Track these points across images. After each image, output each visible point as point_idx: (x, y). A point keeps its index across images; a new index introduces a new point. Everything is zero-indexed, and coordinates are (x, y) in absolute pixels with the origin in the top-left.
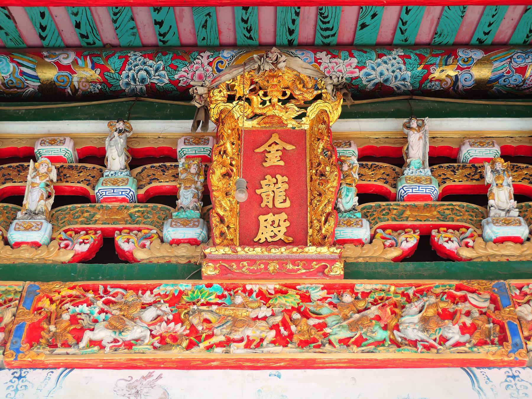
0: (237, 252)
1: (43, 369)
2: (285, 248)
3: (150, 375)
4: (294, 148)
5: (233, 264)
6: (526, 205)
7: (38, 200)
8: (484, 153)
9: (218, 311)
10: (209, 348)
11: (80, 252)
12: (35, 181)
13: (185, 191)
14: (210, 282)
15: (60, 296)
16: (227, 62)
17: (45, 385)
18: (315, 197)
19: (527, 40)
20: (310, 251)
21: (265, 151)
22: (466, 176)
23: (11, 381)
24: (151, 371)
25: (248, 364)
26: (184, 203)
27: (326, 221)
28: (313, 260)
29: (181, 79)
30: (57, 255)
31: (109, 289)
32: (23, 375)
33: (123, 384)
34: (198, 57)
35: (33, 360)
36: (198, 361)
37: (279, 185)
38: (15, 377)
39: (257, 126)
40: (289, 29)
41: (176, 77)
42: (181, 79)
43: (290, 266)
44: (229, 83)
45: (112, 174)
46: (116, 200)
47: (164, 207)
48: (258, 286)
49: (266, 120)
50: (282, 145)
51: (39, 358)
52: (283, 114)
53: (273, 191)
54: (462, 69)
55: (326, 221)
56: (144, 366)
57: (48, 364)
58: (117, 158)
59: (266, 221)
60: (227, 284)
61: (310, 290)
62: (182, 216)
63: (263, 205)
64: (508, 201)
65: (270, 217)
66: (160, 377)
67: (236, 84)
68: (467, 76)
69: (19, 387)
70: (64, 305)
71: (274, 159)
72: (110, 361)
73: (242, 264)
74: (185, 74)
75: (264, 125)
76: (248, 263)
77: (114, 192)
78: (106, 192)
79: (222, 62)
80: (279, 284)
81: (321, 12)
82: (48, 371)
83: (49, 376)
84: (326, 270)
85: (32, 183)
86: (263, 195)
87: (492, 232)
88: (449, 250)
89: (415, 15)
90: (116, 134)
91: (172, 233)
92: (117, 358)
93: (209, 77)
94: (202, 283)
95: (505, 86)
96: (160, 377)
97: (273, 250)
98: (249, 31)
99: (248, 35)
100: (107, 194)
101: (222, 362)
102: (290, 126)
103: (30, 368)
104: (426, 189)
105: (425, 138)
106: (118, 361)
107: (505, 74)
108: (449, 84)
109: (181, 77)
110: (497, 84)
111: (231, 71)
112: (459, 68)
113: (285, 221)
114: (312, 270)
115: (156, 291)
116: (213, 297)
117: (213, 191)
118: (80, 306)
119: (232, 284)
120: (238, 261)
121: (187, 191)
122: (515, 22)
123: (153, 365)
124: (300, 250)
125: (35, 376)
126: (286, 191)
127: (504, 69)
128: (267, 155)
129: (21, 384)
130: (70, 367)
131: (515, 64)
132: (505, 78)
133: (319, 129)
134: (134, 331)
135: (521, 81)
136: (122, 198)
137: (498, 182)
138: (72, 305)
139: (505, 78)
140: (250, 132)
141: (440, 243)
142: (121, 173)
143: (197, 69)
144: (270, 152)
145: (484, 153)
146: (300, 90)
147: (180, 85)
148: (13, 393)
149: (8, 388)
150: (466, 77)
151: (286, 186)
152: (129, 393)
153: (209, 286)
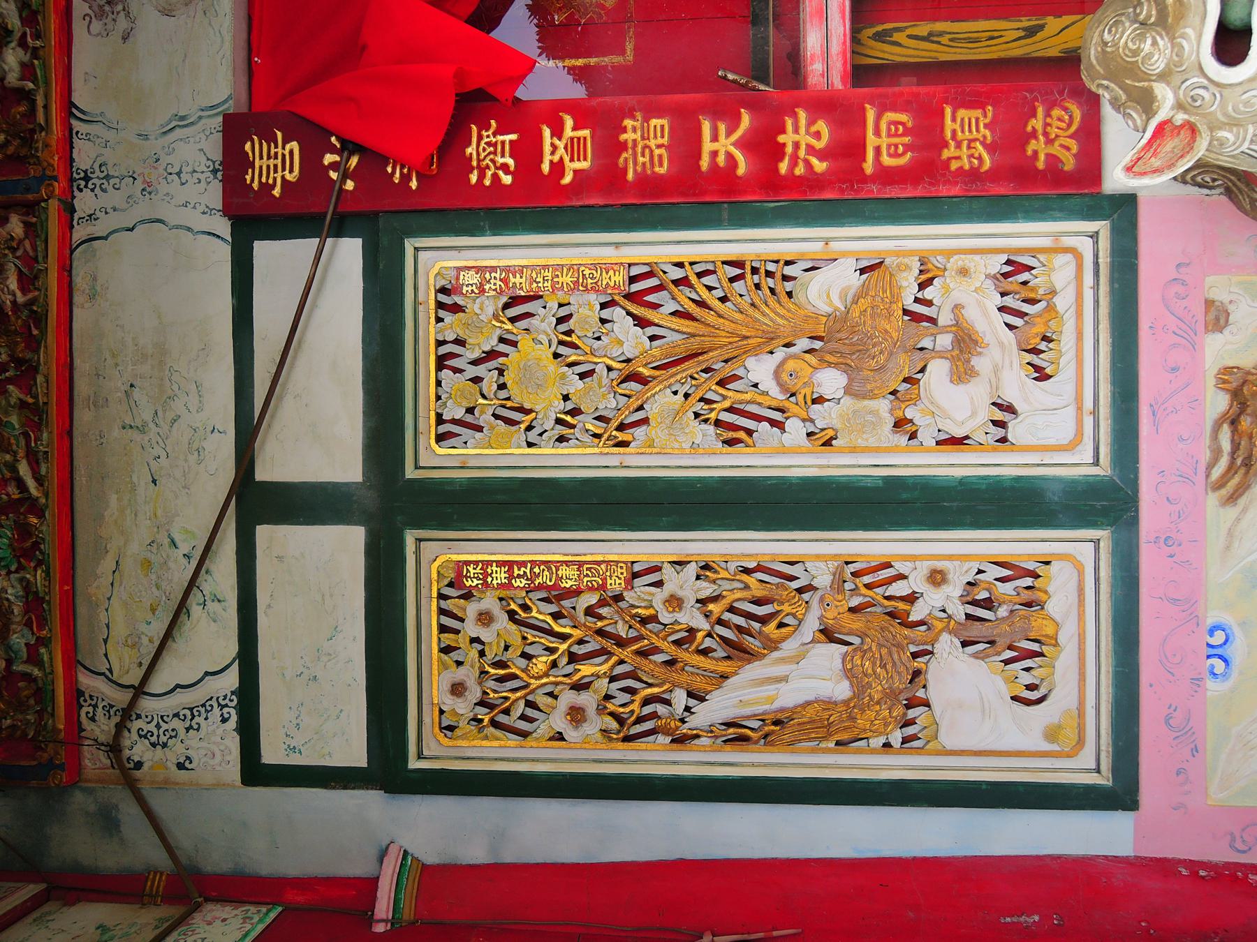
1: (72, 147)
6: (852, 573)
23: (92, 190)
32: (82, 175)
33: (96, 26)
38: (86, 186)
69: (102, 175)
82: (75, 140)
103: (72, 167)
105: (749, 616)
125: (84, 155)
129: (98, 173)
148: (112, 181)
149: (104, 191)
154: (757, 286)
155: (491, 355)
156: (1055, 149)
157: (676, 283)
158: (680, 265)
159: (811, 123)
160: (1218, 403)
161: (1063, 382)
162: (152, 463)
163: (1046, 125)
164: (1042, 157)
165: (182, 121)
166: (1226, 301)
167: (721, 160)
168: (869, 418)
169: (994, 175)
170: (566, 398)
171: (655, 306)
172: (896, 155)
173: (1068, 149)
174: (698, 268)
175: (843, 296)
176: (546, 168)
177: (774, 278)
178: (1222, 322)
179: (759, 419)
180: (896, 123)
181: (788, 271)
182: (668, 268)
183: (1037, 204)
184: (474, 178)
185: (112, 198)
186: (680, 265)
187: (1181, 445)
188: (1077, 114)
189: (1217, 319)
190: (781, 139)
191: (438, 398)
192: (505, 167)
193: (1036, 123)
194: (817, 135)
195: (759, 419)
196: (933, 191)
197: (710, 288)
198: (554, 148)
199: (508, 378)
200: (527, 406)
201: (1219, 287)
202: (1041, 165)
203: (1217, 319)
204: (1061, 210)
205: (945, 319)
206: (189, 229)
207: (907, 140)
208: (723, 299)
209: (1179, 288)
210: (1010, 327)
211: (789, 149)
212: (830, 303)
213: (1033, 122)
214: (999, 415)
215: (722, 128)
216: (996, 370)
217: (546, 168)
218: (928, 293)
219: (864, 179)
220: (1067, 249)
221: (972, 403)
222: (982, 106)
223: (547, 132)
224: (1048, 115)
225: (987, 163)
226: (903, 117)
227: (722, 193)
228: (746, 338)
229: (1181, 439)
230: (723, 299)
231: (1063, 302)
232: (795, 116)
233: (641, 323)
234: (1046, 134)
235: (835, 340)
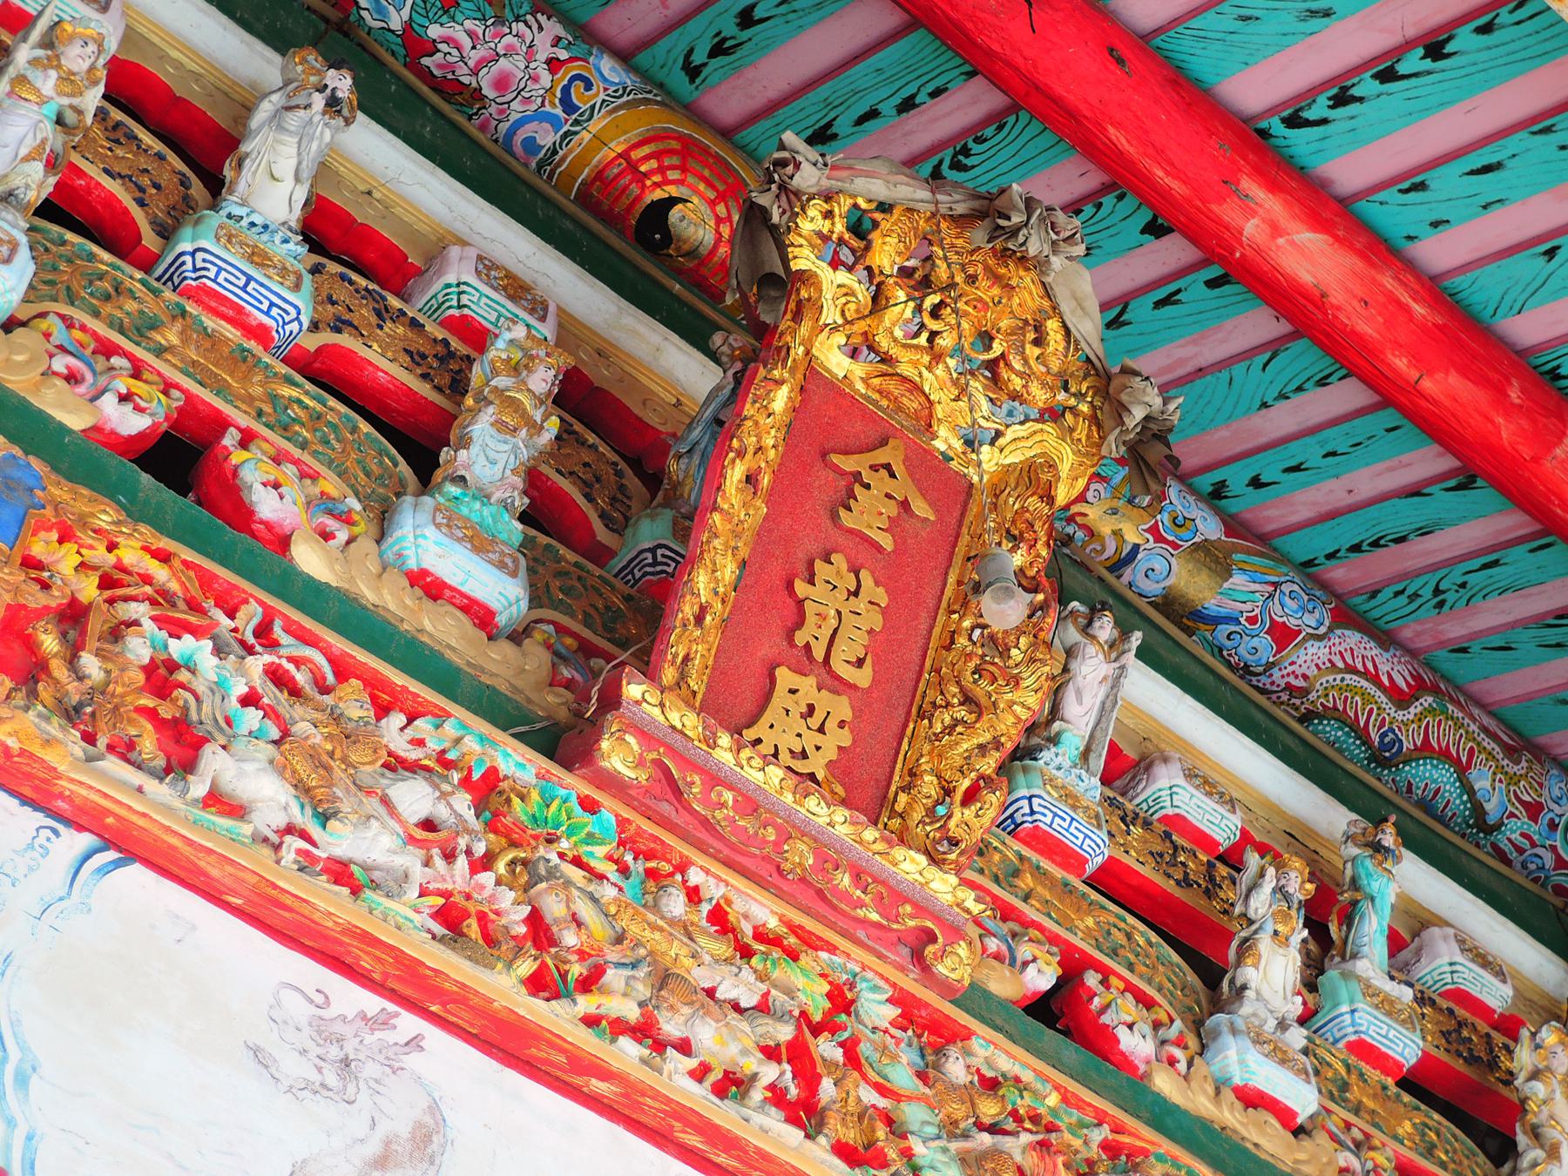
0: (715, 746)
1: (25, 801)
2: (847, 813)
3: (385, 1022)
4: (932, 518)
5: (697, 778)
7: (23, 152)
8: (1207, 816)
9: (613, 910)
10: (591, 1021)
11: (108, 427)
12: (35, 76)
13: (493, 431)
14: (597, 795)
15: (111, 559)
16: (602, 96)
17: (31, 869)
18: (948, 705)
19: (1322, 560)
20: (904, 866)
21: (857, 476)
22: (1151, 853)
24: (392, 1007)
25: (694, 1140)
26: (477, 469)
27: (970, 797)
28: (906, 900)
29: (443, 47)
30: (37, 388)
31: (278, 631)
34: (529, 17)
35: (22, 752)
36: (563, 1051)
37: (861, 604)
39: (860, 387)
40: (829, 124)
41: (434, 31)
42: (443, 47)
43: (845, 880)
44: (864, 205)
45: (253, 224)
46: (237, 318)
47: (376, 440)
48: (722, 890)
49: (892, 385)
50: (902, 487)
51: (50, 756)
52: (944, 398)
53: (839, 613)
54: (1159, 538)
55: (970, 797)
56: (376, 976)
57: (61, 796)
58: (289, 181)
59: (793, 692)
60: (640, 832)
61: (861, 985)
62: (464, 511)
63: (801, 638)
64: (1289, 994)
65: (807, 684)
66: (414, 1043)
67: (883, 223)
68: (1159, 565)
70: (127, 599)
71: (869, 515)
72: (288, 901)
73: (720, 795)
74: (466, 42)
75: (876, 396)
76: (735, 801)
77: (244, 289)
78: (220, 269)
79: (589, 86)
80: (783, 920)
81: (971, 144)
83: (41, 840)
84: (930, 950)
85: (21, 79)
86: (809, 607)
87: (1242, 1062)
88: (1123, 1054)
89: (1172, 323)
90: (319, 101)
91: (434, 549)
92: (322, 905)
93: (527, 100)
94: (573, 785)
95: (1221, 650)
96: (414, 1043)
97: (812, 802)
98: (718, 50)
99: (699, 58)
100: (220, 280)
101: (626, 1095)
102: (939, 444)
104: (1086, 836)
106: (316, 916)
107: (1242, 620)
108: (1105, 556)
109: (447, 40)
110: (1208, 634)
111: (890, 178)
112: (1154, 530)
113: (842, 724)
114: (895, 926)
115: (423, 725)
116: (600, 851)
117: (715, 508)
118: (188, 638)
119: (656, 839)
120: (714, 779)
121: (501, 437)
122: (1351, 500)
123: (408, 992)
124: (880, 847)
126: (871, 632)
127: (1248, 606)
128: (858, 489)
130: (127, 843)
131: (1278, 608)
132: (1237, 629)
133: (1024, 509)
134: (370, 834)
135: (1264, 661)
136: (261, 326)
137: (1280, 928)
138: (153, 618)
139: (1237, 629)
140: (836, 390)
141: (1105, 1019)
142: (286, 241)
143: (510, 52)
144: (868, 487)
145: (1207, 816)
146: (1026, 361)
147: (426, 61)
150: (1157, 567)
151: (877, 621)
152: (320, 1051)
153: (589, 806)
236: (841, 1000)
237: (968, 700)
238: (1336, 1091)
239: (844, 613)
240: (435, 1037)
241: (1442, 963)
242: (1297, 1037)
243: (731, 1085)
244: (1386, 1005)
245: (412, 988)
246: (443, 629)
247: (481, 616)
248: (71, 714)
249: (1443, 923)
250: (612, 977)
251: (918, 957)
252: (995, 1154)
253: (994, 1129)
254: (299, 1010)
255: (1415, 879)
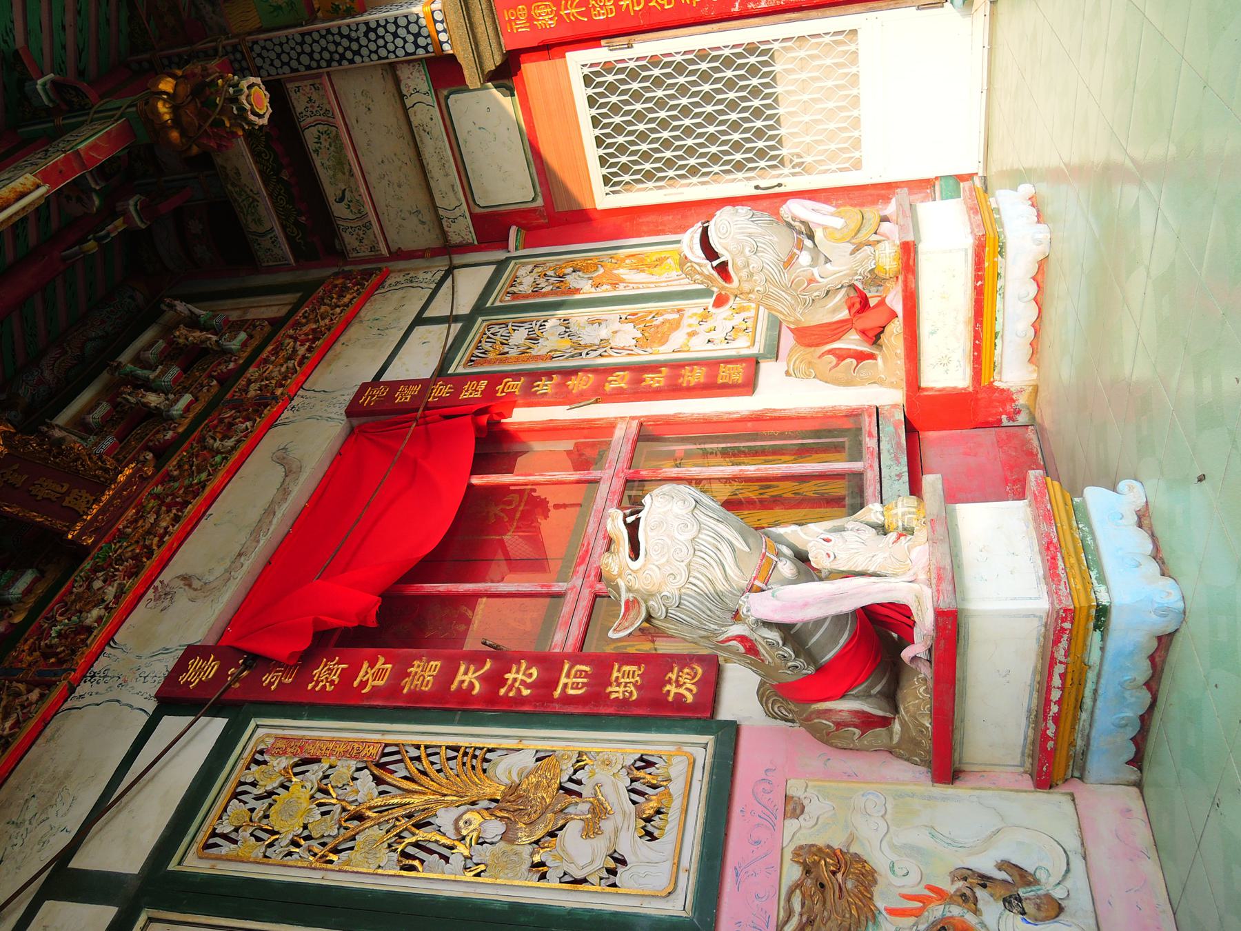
10: (159, 547)
154: (464, 764)
155: (270, 794)
156: (682, 691)
157: (412, 759)
158: (418, 747)
159: (528, 668)
160: (793, 872)
161: (666, 843)
162: (9, 848)
163: (678, 676)
164: (672, 694)
165: (166, 650)
166: (802, 797)
167: (465, 685)
168: (513, 857)
169: (637, 703)
170: (305, 827)
171: (393, 772)
172: (577, 688)
173: (690, 691)
174: (430, 751)
175: (520, 774)
176: (356, 684)
177: (479, 760)
178: (798, 811)
179: (431, 852)
180: (581, 671)
181: (489, 756)
182: (408, 749)
183: (666, 723)
184: (310, 686)
185: (102, 687)
186: (418, 747)
187: (757, 902)
188: (700, 671)
189: (794, 809)
190: (507, 676)
191: (220, 818)
192: (332, 682)
193: (673, 676)
194: (530, 675)
195: (431, 852)
196: (595, 710)
197: (433, 763)
198: (367, 673)
199: (272, 811)
200: (276, 829)
201: (795, 788)
202: (670, 699)
203: (794, 809)
204: (682, 727)
205: (586, 791)
206: (131, 706)
207: (585, 680)
208: (439, 771)
209: (767, 786)
210: (634, 803)
211: (509, 682)
212: (510, 777)
213: (670, 675)
214: (612, 864)
215: (472, 668)
216: (617, 831)
217: (356, 684)
218: (578, 776)
219: (551, 700)
220: (683, 756)
221: (593, 853)
222: (639, 665)
223: (366, 665)
224: (681, 670)
225: (635, 697)
226: (587, 669)
227: (459, 703)
228: (445, 795)
229: (757, 897)
230: (439, 771)
231: (676, 788)
232: (519, 664)
233: (378, 781)
234: (677, 681)
235: (511, 805)
236: (156, 497)
237: (76, 460)
238: (185, 390)
239: (47, 488)
240: (161, 578)
241: (150, 355)
242: (171, 396)
243: (176, 519)
244: (163, 373)
245: (149, 583)
246: (40, 589)
247: (34, 582)
248: (74, 652)
249: (139, 353)
250: (147, 543)
251: (146, 479)
252: (197, 467)
253: (191, 466)
254: (152, 603)
255: (125, 357)
